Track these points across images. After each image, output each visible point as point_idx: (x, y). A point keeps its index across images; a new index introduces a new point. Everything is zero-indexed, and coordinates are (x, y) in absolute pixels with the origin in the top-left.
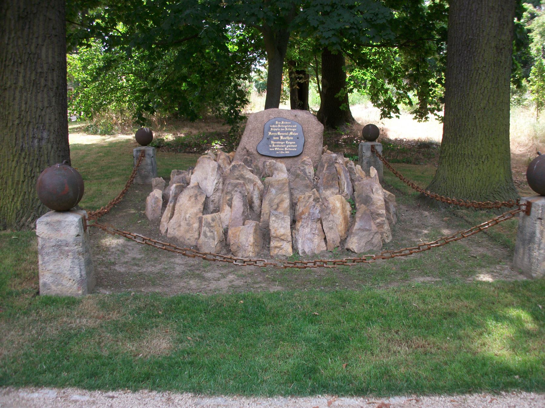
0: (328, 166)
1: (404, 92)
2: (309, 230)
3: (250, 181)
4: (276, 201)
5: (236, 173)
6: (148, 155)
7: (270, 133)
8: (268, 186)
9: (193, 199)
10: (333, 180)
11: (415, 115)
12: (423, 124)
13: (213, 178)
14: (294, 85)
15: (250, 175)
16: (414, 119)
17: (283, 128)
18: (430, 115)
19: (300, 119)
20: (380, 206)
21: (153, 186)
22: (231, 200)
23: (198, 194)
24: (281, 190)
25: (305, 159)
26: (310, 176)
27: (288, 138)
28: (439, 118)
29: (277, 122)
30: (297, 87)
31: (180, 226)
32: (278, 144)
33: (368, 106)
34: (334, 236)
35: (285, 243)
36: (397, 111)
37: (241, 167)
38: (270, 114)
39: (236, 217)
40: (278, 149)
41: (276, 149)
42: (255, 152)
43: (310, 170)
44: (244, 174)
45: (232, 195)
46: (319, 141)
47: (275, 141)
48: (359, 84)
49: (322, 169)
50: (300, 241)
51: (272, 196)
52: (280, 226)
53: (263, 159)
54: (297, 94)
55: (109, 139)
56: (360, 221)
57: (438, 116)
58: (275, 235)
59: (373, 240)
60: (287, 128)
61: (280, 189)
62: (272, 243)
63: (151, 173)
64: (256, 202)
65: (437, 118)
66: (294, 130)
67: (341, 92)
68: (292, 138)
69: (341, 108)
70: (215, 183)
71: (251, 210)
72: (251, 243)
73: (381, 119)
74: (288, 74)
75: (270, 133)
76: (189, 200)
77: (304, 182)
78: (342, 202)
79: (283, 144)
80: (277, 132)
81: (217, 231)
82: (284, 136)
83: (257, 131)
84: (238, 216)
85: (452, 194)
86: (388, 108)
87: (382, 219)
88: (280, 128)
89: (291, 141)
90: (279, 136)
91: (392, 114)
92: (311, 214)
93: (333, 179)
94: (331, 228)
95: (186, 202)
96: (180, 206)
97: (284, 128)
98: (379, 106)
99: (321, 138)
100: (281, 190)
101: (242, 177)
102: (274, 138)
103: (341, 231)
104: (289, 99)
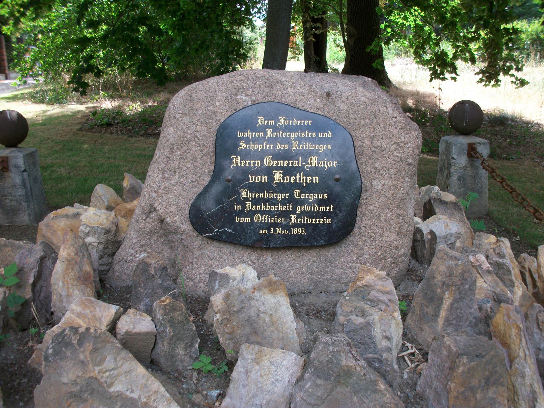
0: (455, 301)
1: (464, 43)
6: (16, 167)
10: (488, 383)
11: (481, 76)
12: (490, 89)
14: (309, 37)
16: (478, 82)
18: (501, 77)
26: (389, 350)
27: (301, 178)
28: (517, 80)
29: (261, 121)
30: (313, 39)
32: (266, 201)
33: (395, 63)
36: (454, 70)
37: (89, 346)
38: (238, 90)
40: (265, 219)
41: (258, 218)
42: (186, 227)
47: (253, 188)
48: (398, 34)
49: (430, 310)
54: (312, 48)
55: (55, 110)
57: (516, 78)
60: (300, 140)
63: (24, 204)
65: (514, 80)
66: (322, 148)
67: (374, 43)
68: (316, 179)
69: (374, 65)
73: (431, 81)
74: (301, 24)
79: (284, 202)
83: (194, 149)
89: (309, 188)
91: (447, 75)
93: (487, 379)
97: (287, 141)
98: (425, 63)
102: (252, 179)
104: (303, 54)
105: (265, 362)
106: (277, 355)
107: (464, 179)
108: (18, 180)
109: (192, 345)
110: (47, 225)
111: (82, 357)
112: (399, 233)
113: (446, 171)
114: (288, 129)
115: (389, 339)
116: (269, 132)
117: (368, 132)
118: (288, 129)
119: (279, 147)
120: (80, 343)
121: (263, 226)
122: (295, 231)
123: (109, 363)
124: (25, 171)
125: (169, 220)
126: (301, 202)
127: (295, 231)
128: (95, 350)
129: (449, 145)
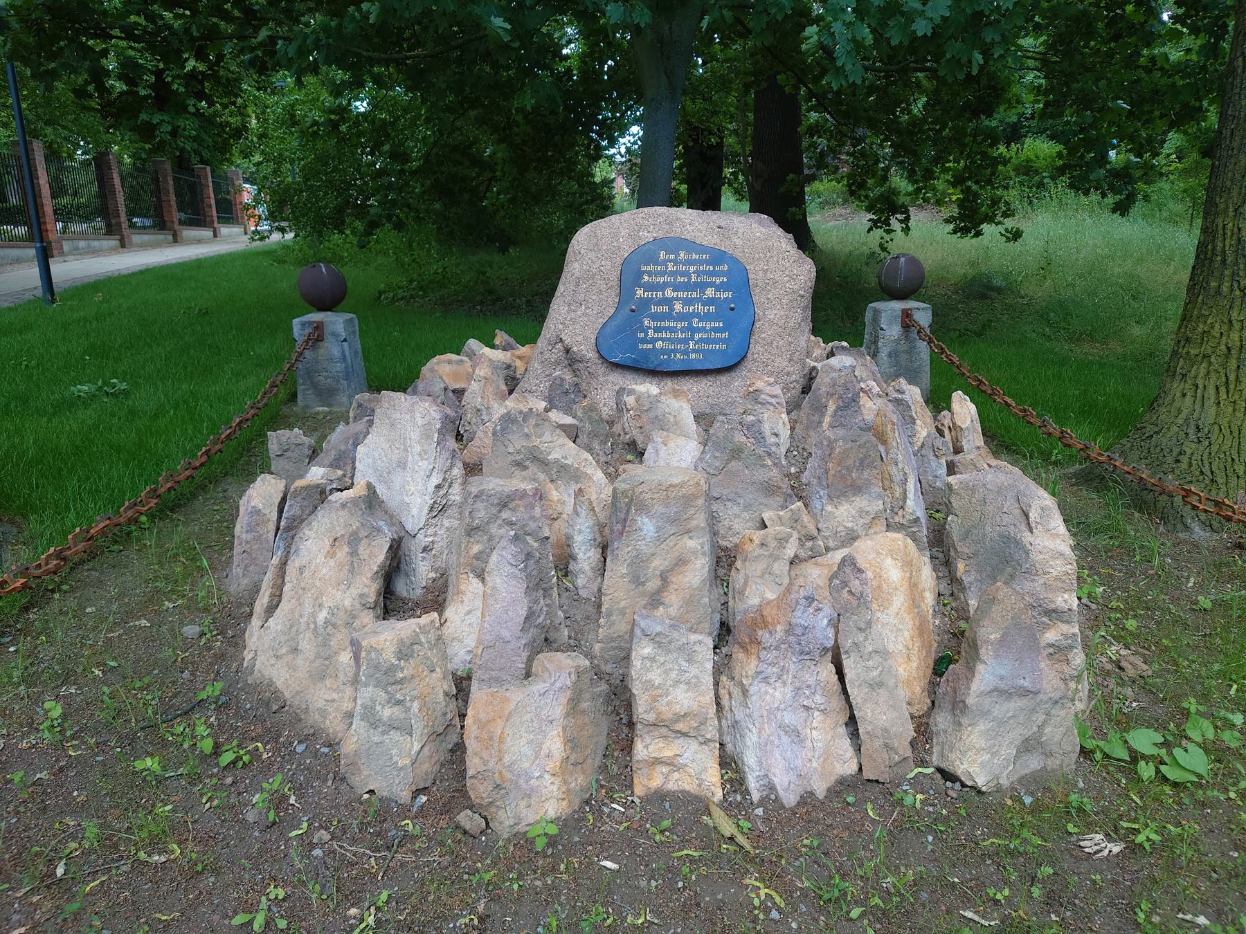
0: (839, 408)
2: (789, 691)
3: (563, 472)
4: (658, 564)
5: (516, 443)
7: (640, 292)
8: (629, 506)
9: (343, 552)
13: (425, 465)
15: (563, 450)
17: (683, 274)
19: (739, 242)
20: (1057, 579)
21: (272, 455)
22: (482, 557)
23: (363, 533)
24: (677, 524)
25: (759, 384)
27: (699, 308)
31: (295, 650)
34: (887, 718)
35: (693, 746)
37: (533, 422)
38: (640, 227)
39: (499, 638)
40: (666, 345)
41: (659, 344)
42: (592, 355)
43: (776, 424)
44: (543, 447)
45: (491, 539)
46: (800, 316)
47: (655, 317)
49: (816, 418)
50: (752, 738)
51: (642, 546)
52: (670, 679)
53: (617, 379)
56: (997, 656)
58: (651, 717)
59: (1048, 730)
60: (698, 273)
61: (674, 521)
62: (639, 747)
64: (586, 557)
70: (431, 489)
71: (562, 610)
72: (554, 764)
75: (640, 292)
76: (331, 555)
77: (761, 475)
78: (908, 564)
80: (662, 287)
81: (421, 698)
82: (687, 302)
83: (601, 284)
84: (506, 634)
85: (1234, 481)
86: (887, 209)
87: (1065, 628)
88: (672, 274)
90: (669, 302)
92: (799, 631)
94: (877, 685)
95: (320, 559)
96: (302, 570)
99: (806, 307)
100: (677, 524)
101: (537, 458)
102: (654, 309)
103: (908, 683)
105: (672, 445)
106: (681, 441)
107: (897, 356)
108: (336, 352)
109: (605, 443)
110: (432, 370)
111: (526, 430)
112: (790, 360)
113: (873, 347)
114: (690, 262)
115: (776, 435)
116: (670, 265)
117: (762, 265)
118: (690, 262)
119: (679, 279)
120: (524, 420)
121: (663, 352)
122: (694, 356)
123: (547, 437)
124: (345, 340)
125: (575, 349)
126: (699, 330)
127: (694, 356)
128: (537, 425)
129: (877, 312)
